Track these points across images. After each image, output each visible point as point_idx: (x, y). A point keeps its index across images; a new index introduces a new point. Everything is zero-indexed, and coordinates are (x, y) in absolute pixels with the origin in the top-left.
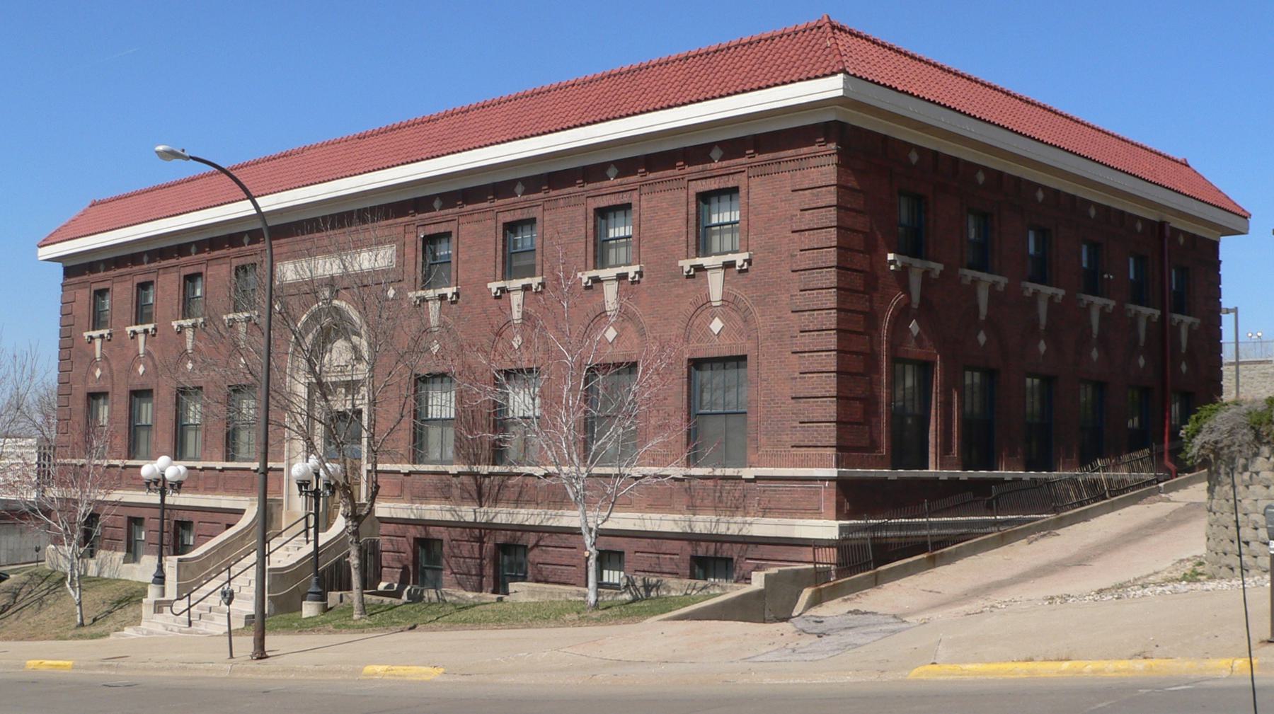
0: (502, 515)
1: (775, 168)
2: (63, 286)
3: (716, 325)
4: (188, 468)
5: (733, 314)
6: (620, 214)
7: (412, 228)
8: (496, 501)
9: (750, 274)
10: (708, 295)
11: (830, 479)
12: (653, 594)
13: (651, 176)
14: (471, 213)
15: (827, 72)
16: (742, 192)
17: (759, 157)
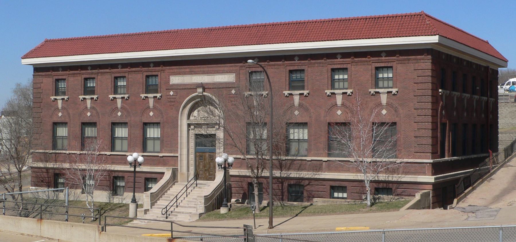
0: (294, 174)
1: (407, 62)
2: (33, 75)
3: (119, 114)
4: (234, 158)
5: (391, 109)
6: (122, 79)
7: (244, 68)
8: (289, 169)
9: (397, 96)
10: (294, 103)
11: (429, 163)
12: (377, 201)
13: (356, 59)
14: (274, 65)
15: (363, 37)
16: (159, 75)
17: (401, 58)
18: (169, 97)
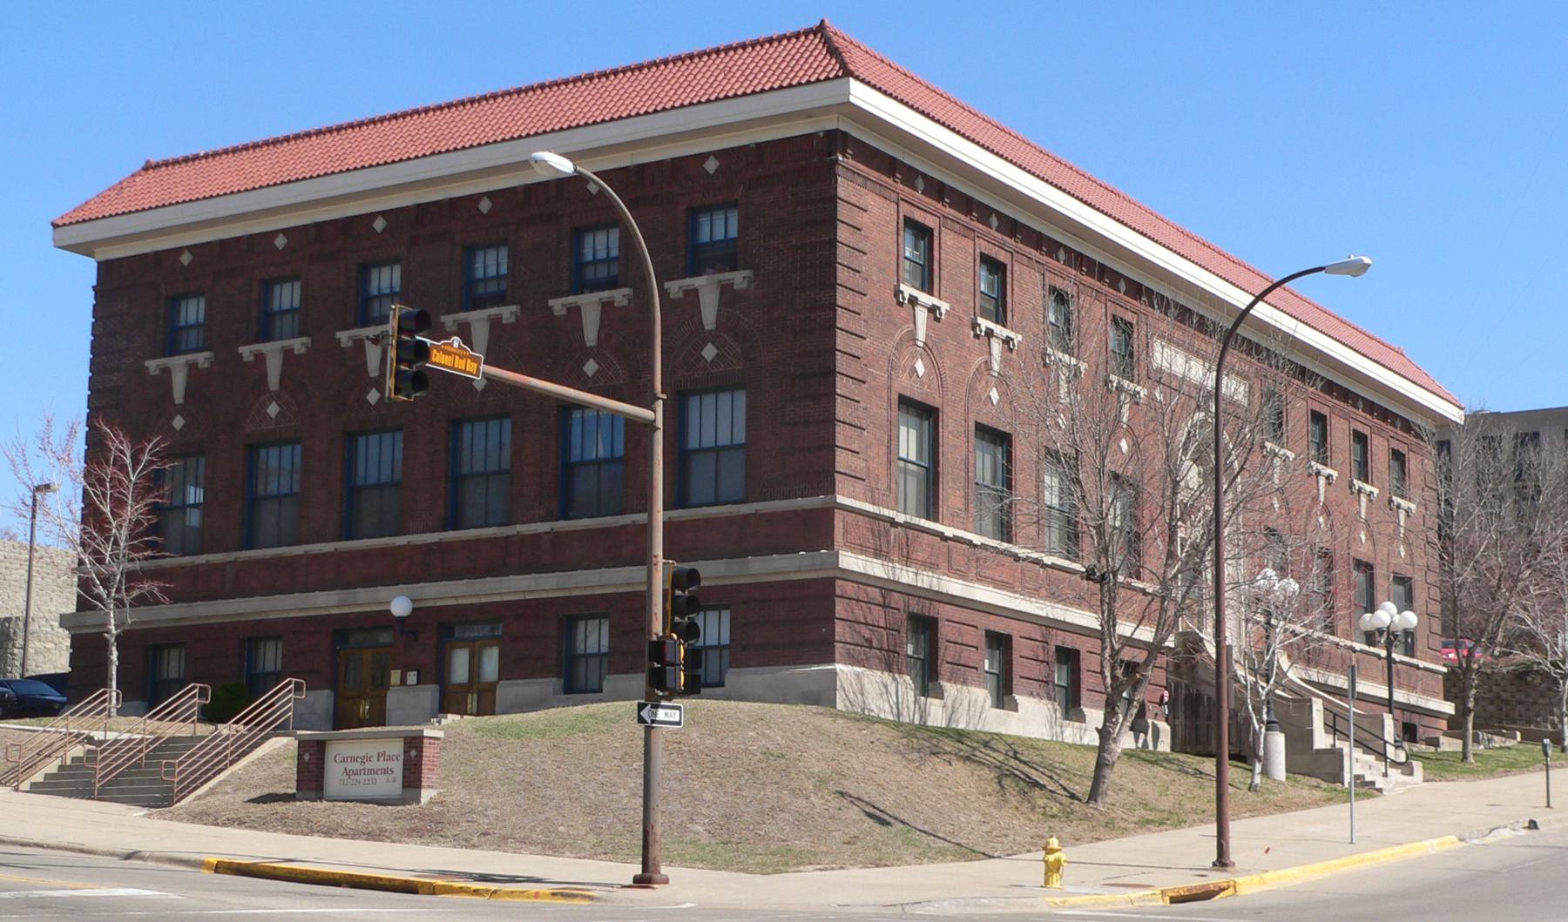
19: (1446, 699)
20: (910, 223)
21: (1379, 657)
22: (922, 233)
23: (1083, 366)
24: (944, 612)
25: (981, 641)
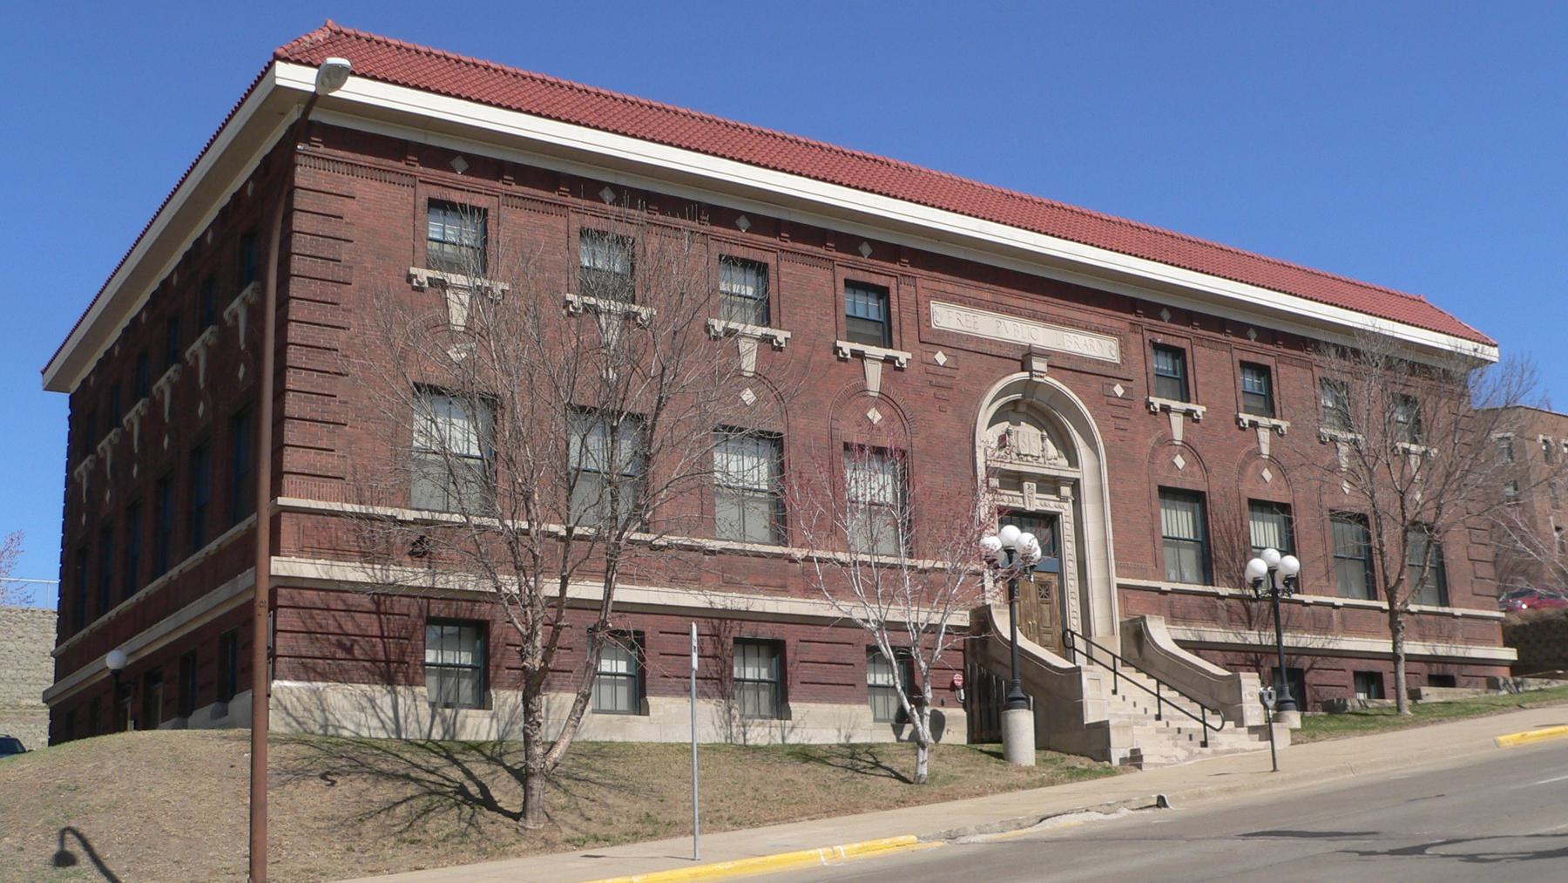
18: (931, 368)
19: (1507, 644)
20: (1245, 365)
21: (1380, 609)
22: (1263, 371)
23: (1360, 437)
24: (791, 635)
25: (1349, 680)
